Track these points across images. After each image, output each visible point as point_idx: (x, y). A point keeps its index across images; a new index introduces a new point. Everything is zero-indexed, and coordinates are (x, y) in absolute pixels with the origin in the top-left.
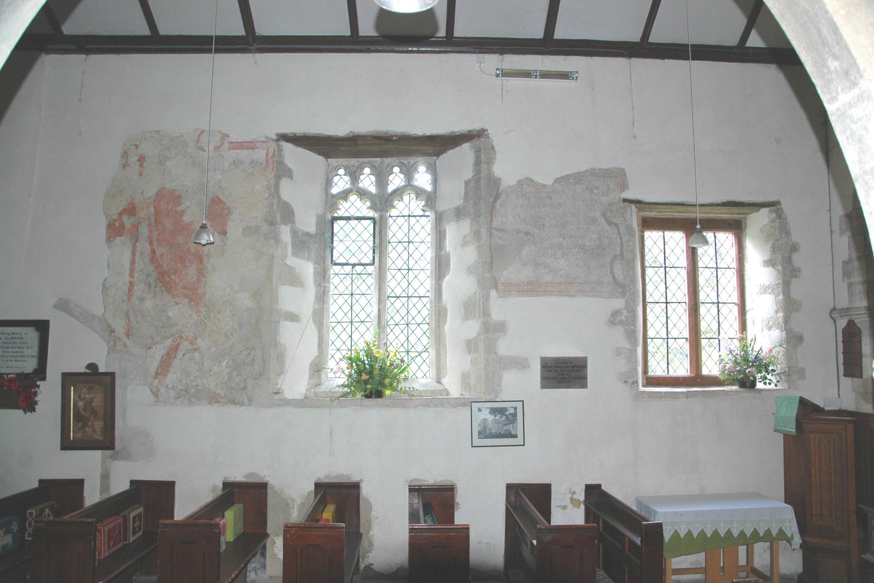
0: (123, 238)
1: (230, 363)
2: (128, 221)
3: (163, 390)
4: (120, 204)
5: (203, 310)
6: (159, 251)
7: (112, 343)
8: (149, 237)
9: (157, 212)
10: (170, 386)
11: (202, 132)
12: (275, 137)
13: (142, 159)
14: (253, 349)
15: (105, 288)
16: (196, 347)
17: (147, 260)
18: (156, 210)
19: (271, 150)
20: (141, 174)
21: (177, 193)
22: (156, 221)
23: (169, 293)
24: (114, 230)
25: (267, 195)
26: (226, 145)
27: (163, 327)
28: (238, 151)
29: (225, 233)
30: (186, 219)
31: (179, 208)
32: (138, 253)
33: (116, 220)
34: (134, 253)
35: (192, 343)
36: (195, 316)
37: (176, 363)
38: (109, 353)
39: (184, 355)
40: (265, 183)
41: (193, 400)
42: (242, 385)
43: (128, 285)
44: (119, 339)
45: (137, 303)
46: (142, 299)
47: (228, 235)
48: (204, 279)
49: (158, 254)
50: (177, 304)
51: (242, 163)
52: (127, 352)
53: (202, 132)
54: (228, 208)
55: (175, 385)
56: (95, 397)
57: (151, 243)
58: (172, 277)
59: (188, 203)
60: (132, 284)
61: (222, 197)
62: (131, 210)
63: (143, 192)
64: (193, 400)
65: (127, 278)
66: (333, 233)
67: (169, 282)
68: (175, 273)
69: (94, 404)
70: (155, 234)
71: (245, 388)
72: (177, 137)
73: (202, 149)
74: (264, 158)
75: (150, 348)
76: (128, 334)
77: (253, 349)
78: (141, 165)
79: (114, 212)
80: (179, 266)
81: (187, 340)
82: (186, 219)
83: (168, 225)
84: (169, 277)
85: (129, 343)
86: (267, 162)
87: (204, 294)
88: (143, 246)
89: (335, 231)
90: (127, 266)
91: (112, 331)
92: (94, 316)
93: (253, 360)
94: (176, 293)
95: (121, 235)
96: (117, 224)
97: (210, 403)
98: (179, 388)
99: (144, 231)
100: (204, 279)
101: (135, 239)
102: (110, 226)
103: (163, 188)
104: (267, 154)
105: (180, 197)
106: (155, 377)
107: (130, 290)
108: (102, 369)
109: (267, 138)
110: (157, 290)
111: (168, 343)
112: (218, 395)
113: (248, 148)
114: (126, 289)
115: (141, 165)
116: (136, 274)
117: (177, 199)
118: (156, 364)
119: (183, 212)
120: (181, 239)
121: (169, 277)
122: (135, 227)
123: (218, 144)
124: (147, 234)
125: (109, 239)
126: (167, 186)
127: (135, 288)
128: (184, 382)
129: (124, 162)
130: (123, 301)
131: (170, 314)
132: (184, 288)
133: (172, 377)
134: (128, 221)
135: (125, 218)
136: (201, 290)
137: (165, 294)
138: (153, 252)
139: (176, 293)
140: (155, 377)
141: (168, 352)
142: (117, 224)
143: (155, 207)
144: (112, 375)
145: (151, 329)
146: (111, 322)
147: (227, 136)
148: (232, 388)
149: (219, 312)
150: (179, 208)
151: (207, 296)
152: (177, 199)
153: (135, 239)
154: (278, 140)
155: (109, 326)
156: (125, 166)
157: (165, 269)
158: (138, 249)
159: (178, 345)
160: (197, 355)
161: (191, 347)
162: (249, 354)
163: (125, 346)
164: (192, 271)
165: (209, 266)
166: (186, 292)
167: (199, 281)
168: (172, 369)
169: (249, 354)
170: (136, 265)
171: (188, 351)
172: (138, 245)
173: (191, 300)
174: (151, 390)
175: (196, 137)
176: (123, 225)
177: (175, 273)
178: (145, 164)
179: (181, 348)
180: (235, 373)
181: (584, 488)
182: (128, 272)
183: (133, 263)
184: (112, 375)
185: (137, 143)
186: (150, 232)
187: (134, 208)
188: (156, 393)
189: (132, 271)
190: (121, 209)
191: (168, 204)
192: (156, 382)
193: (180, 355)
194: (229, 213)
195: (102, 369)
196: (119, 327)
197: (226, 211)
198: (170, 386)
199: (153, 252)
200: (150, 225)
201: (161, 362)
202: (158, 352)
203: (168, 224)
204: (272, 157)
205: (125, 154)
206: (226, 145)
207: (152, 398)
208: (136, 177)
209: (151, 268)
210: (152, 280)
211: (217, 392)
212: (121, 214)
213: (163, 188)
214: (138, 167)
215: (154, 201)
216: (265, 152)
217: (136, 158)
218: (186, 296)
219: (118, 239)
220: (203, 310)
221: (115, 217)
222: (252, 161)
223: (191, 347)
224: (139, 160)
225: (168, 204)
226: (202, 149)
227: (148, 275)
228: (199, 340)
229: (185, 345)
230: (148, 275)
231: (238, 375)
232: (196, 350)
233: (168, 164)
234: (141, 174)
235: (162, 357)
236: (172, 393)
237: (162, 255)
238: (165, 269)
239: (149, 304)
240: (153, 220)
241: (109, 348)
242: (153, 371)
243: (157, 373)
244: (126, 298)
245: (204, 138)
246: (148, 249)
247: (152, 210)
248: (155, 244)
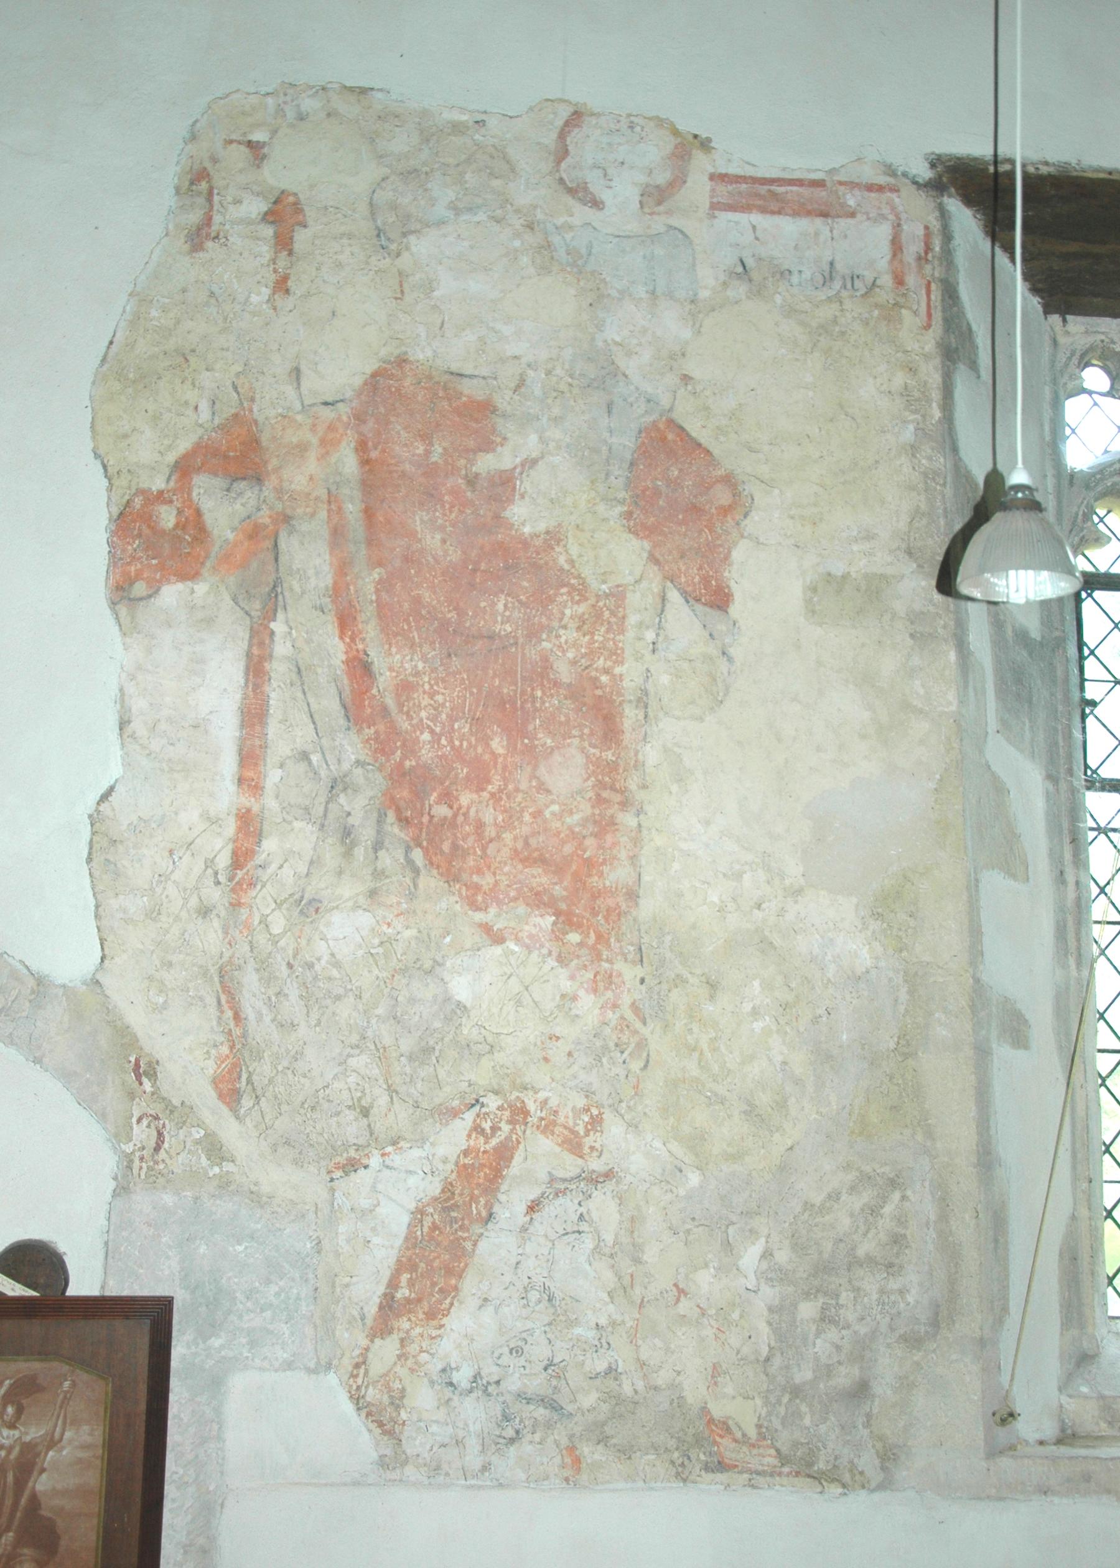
0: (201, 588)
1: (783, 1256)
2: (223, 510)
3: (423, 1398)
4: (190, 417)
5: (630, 973)
6: (389, 664)
7: (142, 1134)
8: (337, 591)
9: (375, 473)
10: (462, 1377)
11: (577, 117)
12: (925, 173)
13: (283, 215)
14: (893, 1183)
15: (104, 844)
16: (596, 1165)
17: (329, 704)
18: (365, 462)
19: (913, 230)
20: (282, 285)
21: (471, 389)
22: (368, 513)
23: (451, 877)
24: (152, 544)
25: (908, 434)
26: (698, 188)
27: (424, 1053)
28: (756, 218)
29: (718, 598)
30: (526, 516)
31: (486, 464)
32: (279, 669)
33: (161, 497)
34: (256, 669)
35: (573, 1145)
36: (587, 1004)
37: (495, 1246)
38: (122, 1190)
39: (533, 1208)
40: (900, 379)
41: (589, 1451)
42: (846, 1376)
43: (230, 828)
44: (183, 1114)
45: (278, 923)
46: (308, 907)
47: (734, 610)
48: (628, 820)
49: (385, 680)
50: (498, 939)
51: (784, 274)
52: (225, 1184)
53: (577, 117)
54: (729, 480)
55: (491, 1371)
56: (52, 1443)
57: (346, 622)
58: (465, 798)
59: (531, 444)
60: (249, 827)
61: (695, 428)
62: (236, 453)
63: (296, 374)
64: (589, 1451)
65: (226, 796)
66: (1081, 644)
67: (451, 823)
68: (479, 781)
69: (42, 1484)
70: (367, 582)
71: (861, 1390)
72: (457, 128)
73: (581, 193)
74: (883, 264)
75: (352, 1166)
76: (230, 1089)
77: (893, 1183)
78: (284, 243)
79: (151, 457)
80: (498, 745)
81: (547, 1127)
82: (526, 516)
83: (433, 541)
84: (447, 798)
85: (232, 1132)
86: (899, 281)
87: (633, 896)
88: (306, 636)
89: (1090, 637)
90: (226, 731)
91: (144, 1070)
92: (41, 981)
93: (897, 1240)
94: (486, 881)
95: (189, 575)
96: (167, 517)
97: (682, 1476)
98: (513, 1384)
99: (309, 560)
100: (628, 820)
101: (266, 601)
102: (131, 522)
103: (402, 361)
104: (896, 246)
105: (485, 408)
106: (381, 1328)
107: (240, 858)
108: (82, 1283)
109: (890, 171)
110: (386, 860)
111: (452, 1140)
112: (725, 1427)
113: (803, 211)
114: (219, 846)
115: (284, 243)
116: (273, 777)
117: (477, 419)
118: (383, 1254)
119: (504, 485)
120: (502, 613)
121: (447, 798)
122: (263, 538)
123: (662, 178)
124: (329, 581)
125: (124, 592)
126: (420, 354)
127: (270, 845)
128: (539, 1351)
129: (194, 217)
130: (205, 911)
131: (461, 988)
132: (528, 857)
133: (468, 1330)
134: (223, 510)
135: (206, 491)
136: (618, 875)
137: (430, 881)
138: (360, 668)
139: (486, 881)
140: (381, 1328)
141: (448, 1188)
142: (167, 517)
143: (362, 447)
144: (157, 1316)
145: (360, 1061)
146: (137, 1018)
147: (705, 145)
148: (796, 1392)
149: (713, 986)
150: (486, 464)
151: (648, 907)
152: (477, 419)
153: (266, 601)
154: (936, 187)
155: (125, 1037)
156: (200, 236)
157: (426, 754)
158: (281, 648)
159: (504, 1154)
160: (603, 1206)
161: (570, 1165)
162: (873, 1211)
163: (215, 1149)
164: (566, 773)
165: (651, 755)
166: (539, 878)
167: (604, 826)
168: (469, 1285)
169: (873, 1211)
170: (273, 728)
171: (557, 1187)
172: (278, 626)
173: (567, 920)
174: (357, 1399)
175: (550, 139)
176: (194, 525)
177: (479, 781)
178: (301, 238)
179: (516, 1166)
180: (808, 1310)
181: (167, 1294)
182: (229, 764)
183: (254, 715)
184: (157, 1316)
185: (258, 136)
186: (342, 568)
187: (253, 444)
188: (384, 1418)
189: (250, 758)
190: (184, 445)
191: (426, 437)
192: (386, 1350)
193: (512, 1203)
194: (737, 506)
195: (82, 1283)
196: (186, 1052)
197: (723, 496)
198: (462, 1377)
199: (360, 668)
200: (337, 534)
201: (411, 1240)
202: (397, 1192)
203: (433, 536)
204: (922, 259)
205: (198, 181)
206: (698, 188)
207: (366, 1443)
208: (260, 297)
209: (351, 748)
210: (358, 806)
211: (717, 1411)
212: (184, 469)
213: (402, 361)
214: (265, 250)
215: (359, 417)
216: (884, 231)
217: (255, 207)
218: (539, 900)
219: (172, 594)
220: (630, 973)
221: (158, 483)
222: (829, 275)
223: (570, 1165)
224: (272, 216)
225: (426, 437)
226: (581, 193)
227: (338, 785)
228: (614, 1130)
229: (539, 1156)
230: (338, 785)
231: (826, 1319)
232: (596, 1180)
233: (421, 247)
234: (282, 285)
235: (419, 1213)
236: (475, 1414)
237: (405, 688)
238: (426, 754)
239: (346, 931)
240: (353, 509)
241: (127, 1162)
242: (368, 1291)
243: (389, 1307)
244: (216, 895)
245: (587, 146)
246: (337, 650)
247: (348, 462)
248: (370, 630)
